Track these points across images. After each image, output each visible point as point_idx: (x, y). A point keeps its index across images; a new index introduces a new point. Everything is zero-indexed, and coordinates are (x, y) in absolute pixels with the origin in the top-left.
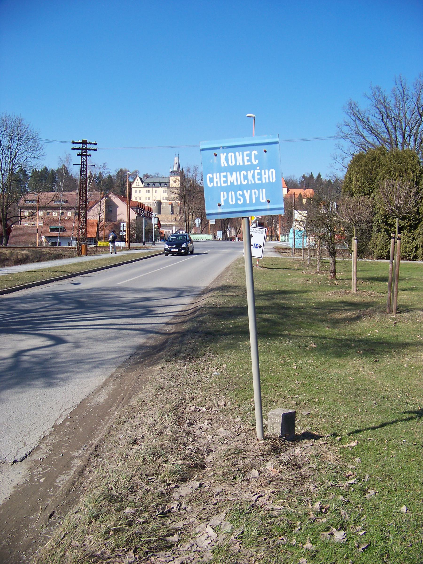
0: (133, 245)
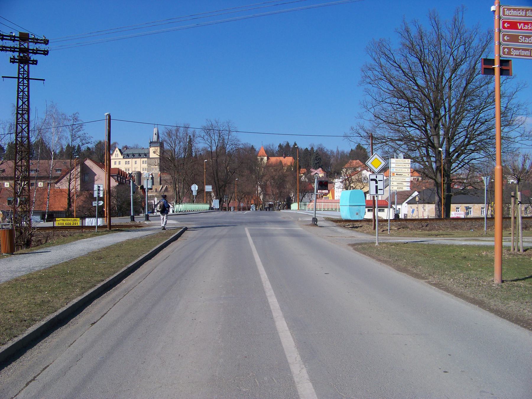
0: (116, 221)
